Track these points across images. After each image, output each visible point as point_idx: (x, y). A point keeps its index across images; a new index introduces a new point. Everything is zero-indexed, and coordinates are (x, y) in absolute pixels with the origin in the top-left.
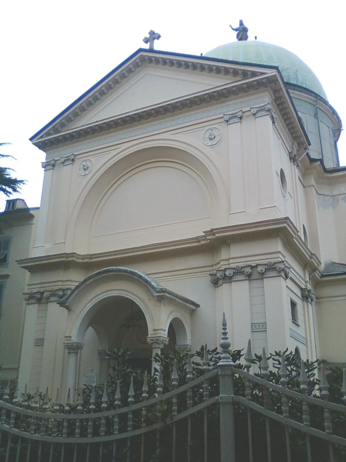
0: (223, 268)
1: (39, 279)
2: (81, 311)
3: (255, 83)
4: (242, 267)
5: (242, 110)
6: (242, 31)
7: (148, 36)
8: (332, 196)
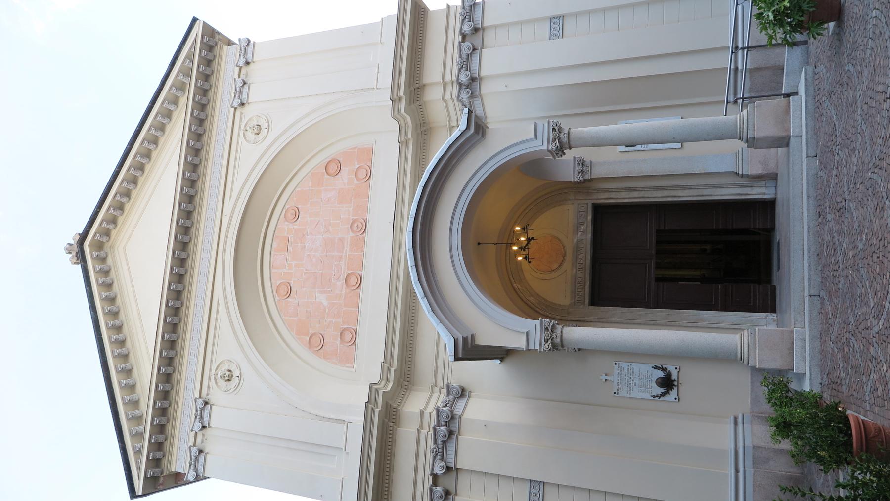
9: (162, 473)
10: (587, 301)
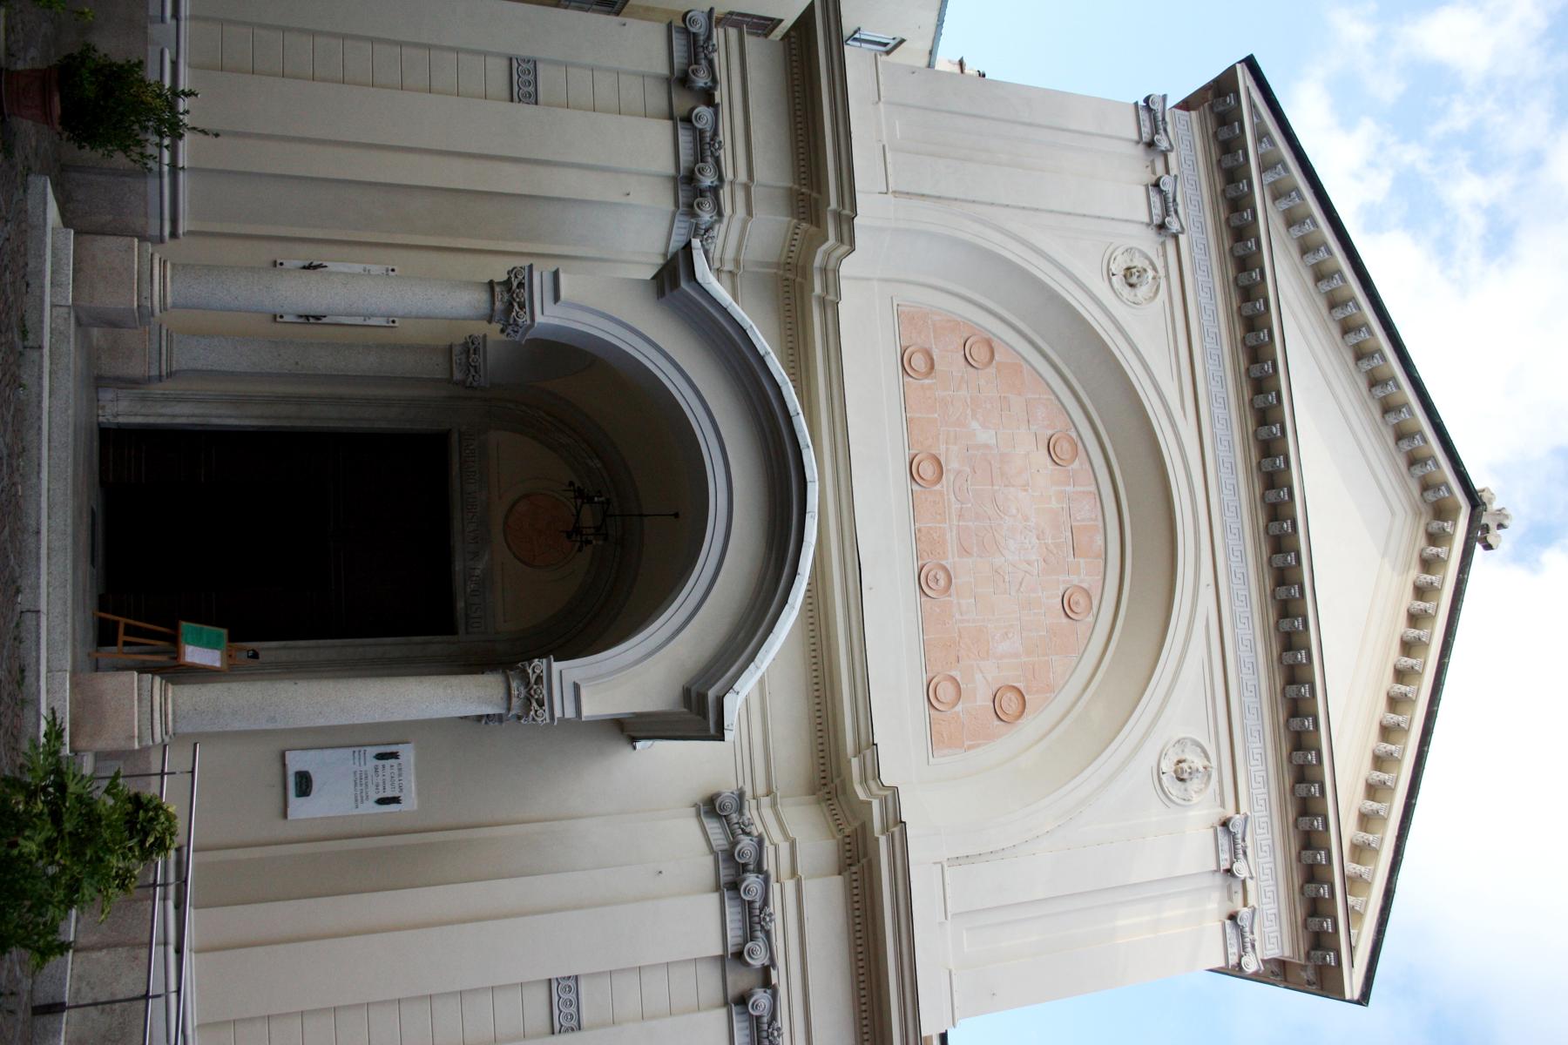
5: (1182, 232)
9: (1211, 107)
10: (455, 437)
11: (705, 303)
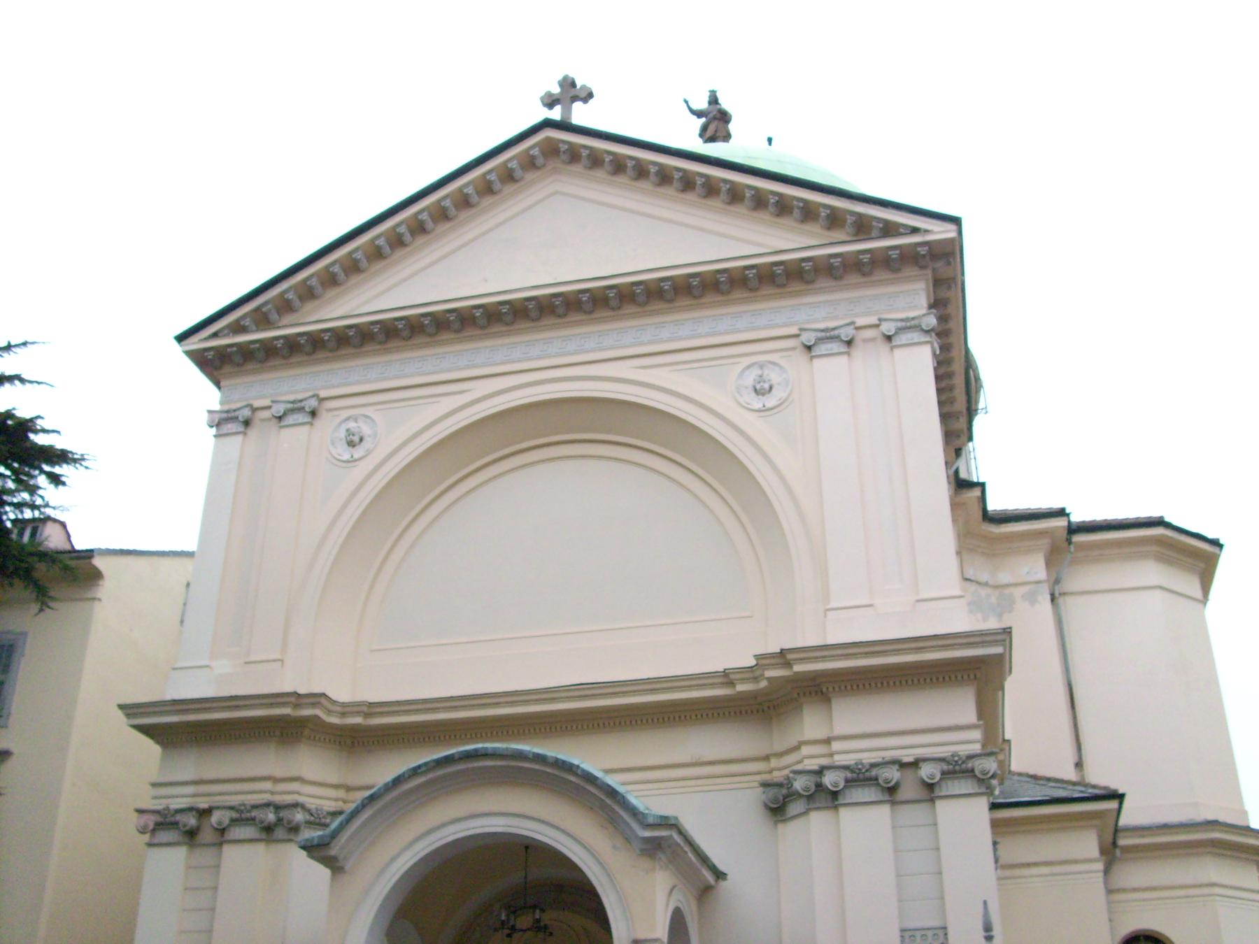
0: (812, 764)
1: (191, 765)
2: (382, 871)
3: (894, 254)
4: (873, 765)
5: (853, 323)
6: (715, 118)
7: (556, 90)
8: (996, 587)
11: (499, 763)
